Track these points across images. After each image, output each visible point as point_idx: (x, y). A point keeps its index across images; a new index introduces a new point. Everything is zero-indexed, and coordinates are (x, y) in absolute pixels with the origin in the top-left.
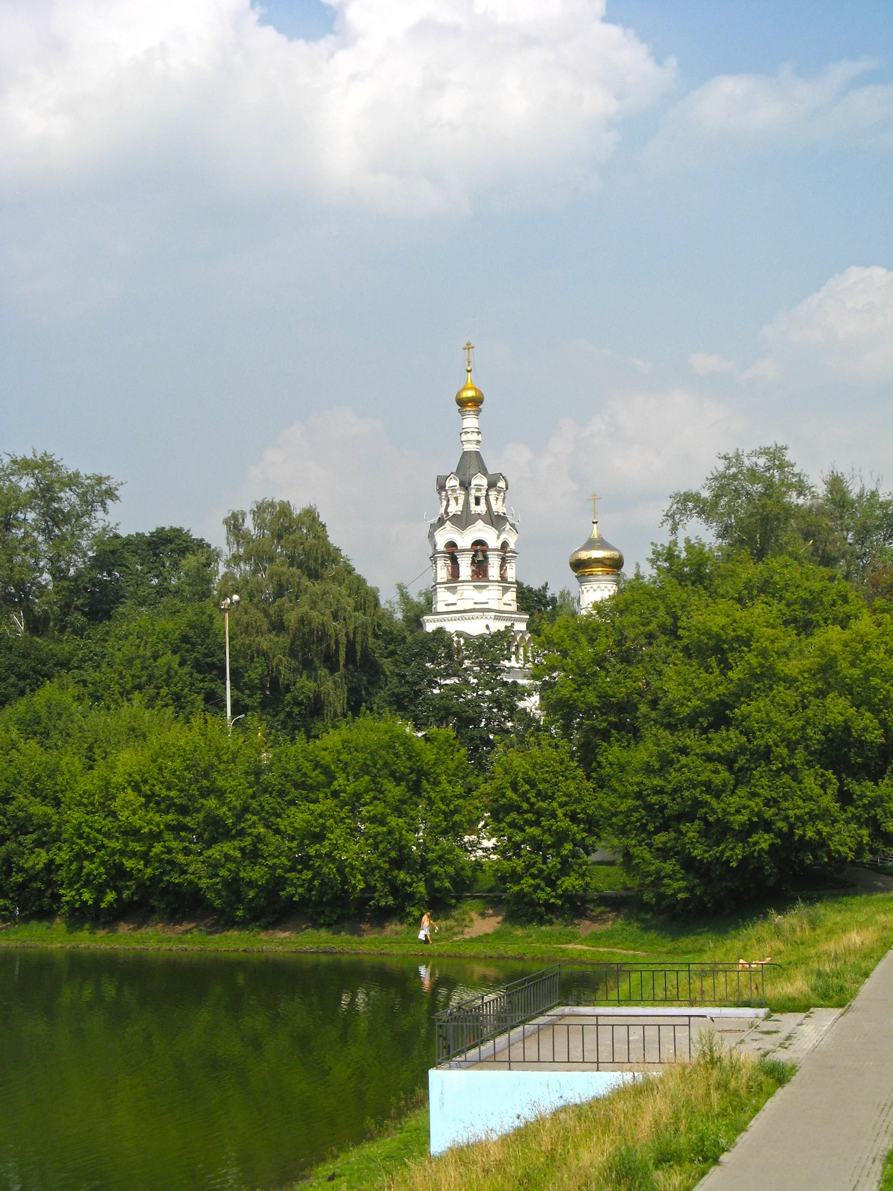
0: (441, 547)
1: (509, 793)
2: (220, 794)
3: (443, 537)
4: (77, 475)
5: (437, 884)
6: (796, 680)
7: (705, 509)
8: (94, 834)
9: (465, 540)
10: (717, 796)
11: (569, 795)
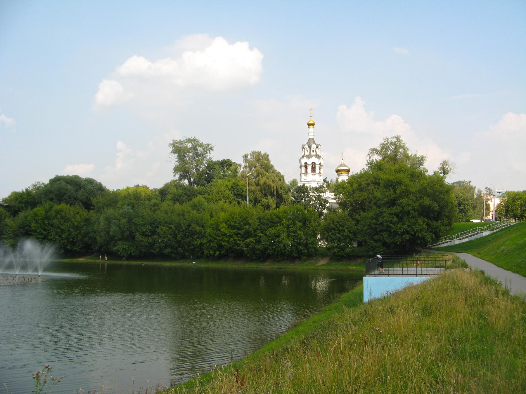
0: (303, 164)
1: (332, 225)
2: (250, 225)
3: (304, 161)
4: (202, 143)
5: (310, 250)
6: (415, 193)
7: (377, 152)
8: (214, 236)
9: (310, 162)
10: (394, 225)
11: (348, 226)
